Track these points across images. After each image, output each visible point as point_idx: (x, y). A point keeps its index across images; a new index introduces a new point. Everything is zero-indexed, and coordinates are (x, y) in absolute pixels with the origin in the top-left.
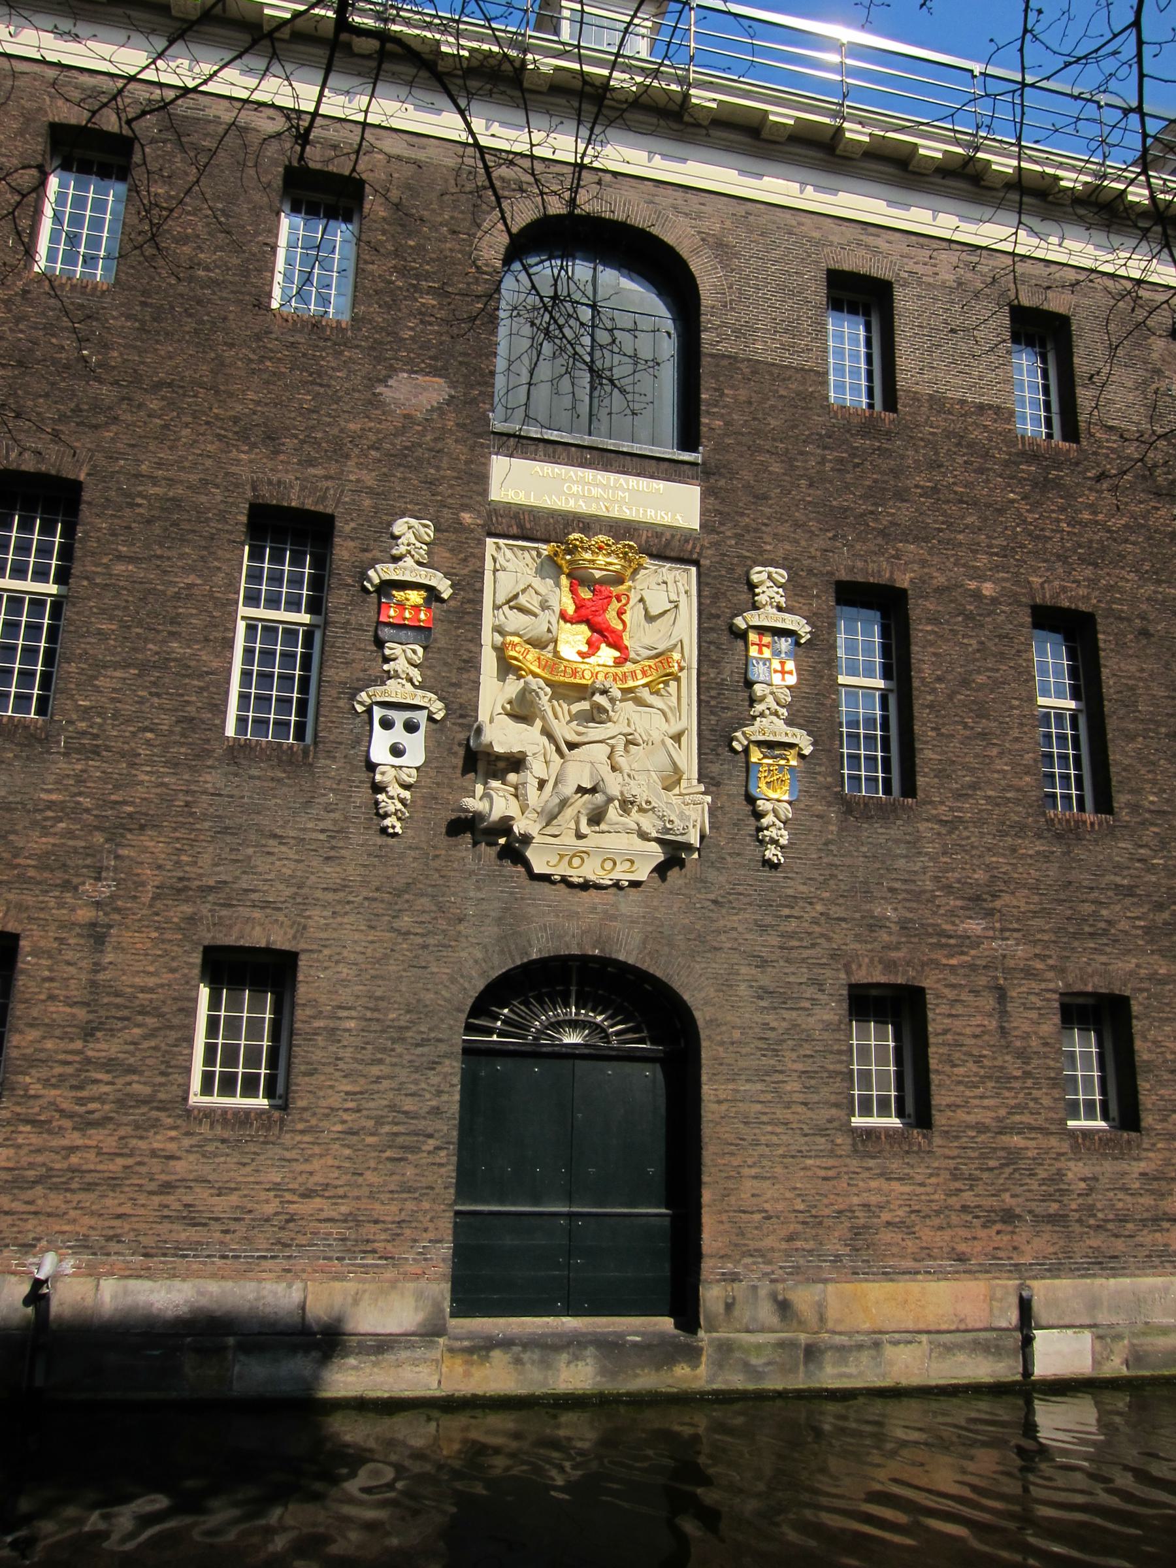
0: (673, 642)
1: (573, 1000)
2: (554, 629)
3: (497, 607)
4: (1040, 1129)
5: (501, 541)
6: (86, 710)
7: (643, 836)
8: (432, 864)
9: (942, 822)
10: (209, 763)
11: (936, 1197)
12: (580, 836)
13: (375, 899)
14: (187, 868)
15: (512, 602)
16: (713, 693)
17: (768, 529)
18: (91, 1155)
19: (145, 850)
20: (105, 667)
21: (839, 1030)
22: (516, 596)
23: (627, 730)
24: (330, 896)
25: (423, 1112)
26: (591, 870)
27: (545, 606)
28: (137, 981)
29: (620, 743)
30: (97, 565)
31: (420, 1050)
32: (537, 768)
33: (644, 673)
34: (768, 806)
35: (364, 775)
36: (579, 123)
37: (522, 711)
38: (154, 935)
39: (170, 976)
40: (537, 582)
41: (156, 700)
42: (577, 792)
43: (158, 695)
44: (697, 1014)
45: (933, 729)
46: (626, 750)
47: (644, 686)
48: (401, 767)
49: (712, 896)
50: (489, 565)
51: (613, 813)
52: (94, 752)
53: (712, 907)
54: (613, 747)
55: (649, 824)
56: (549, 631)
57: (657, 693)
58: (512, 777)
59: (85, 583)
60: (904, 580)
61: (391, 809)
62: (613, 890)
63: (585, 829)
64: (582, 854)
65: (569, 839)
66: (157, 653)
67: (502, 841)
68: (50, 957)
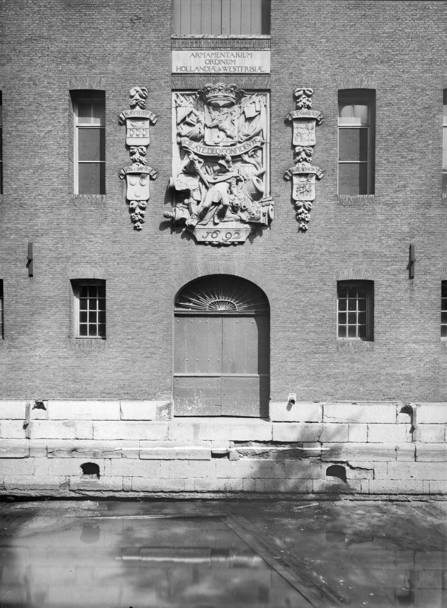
1: (262, 375)
2: (202, 133)
3: (178, 124)
4: (427, 341)
5: (178, 93)
6: (16, 189)
8: (156, 241)
9: (387, 204)
10: (64, 206)
11: (374, 369)
12: (215, 224)
13: (134, 257)
14: (61, 250)
16: (277, 153)
17: (304, 68)
18: (37, 358)
19: (45, 243)
20: (20, 170)
21: (332, 300)
22: (185, 118)
23: (237, 175)
24: (116, 257)
26: (220, 238)
28: (47, 294)
29: (234, 181)
30: (12, 127)
31: (154, 316)
32: (196, 195)
33: (245, 147)
34: (301, 204)
35: (125, 206)
36: (172, 201)
37: (190, 171)
38: (52, 276)
39: (59, 291)
40: (195, 111)
41: (41, 182)
43: (41, 180)
45: (385, 160)
46: (237, 184)
48: (140, 201)
49: (276, 246)
50: (174, 105)
51: (228, 213)
52: (21, 206)
53: (276, 250)
54: (230, 183)
55: (245, 216)
56: (200, 133)
57: (252, 156)
58: (186, 201)
59: (8, 136)
60: (372, 85)
61: (137, 219)
62: (232, 246)
63: (217, 221)
64: (216, 232)
66: (39, 162)
67: (184, 229)
68: (15, 287)
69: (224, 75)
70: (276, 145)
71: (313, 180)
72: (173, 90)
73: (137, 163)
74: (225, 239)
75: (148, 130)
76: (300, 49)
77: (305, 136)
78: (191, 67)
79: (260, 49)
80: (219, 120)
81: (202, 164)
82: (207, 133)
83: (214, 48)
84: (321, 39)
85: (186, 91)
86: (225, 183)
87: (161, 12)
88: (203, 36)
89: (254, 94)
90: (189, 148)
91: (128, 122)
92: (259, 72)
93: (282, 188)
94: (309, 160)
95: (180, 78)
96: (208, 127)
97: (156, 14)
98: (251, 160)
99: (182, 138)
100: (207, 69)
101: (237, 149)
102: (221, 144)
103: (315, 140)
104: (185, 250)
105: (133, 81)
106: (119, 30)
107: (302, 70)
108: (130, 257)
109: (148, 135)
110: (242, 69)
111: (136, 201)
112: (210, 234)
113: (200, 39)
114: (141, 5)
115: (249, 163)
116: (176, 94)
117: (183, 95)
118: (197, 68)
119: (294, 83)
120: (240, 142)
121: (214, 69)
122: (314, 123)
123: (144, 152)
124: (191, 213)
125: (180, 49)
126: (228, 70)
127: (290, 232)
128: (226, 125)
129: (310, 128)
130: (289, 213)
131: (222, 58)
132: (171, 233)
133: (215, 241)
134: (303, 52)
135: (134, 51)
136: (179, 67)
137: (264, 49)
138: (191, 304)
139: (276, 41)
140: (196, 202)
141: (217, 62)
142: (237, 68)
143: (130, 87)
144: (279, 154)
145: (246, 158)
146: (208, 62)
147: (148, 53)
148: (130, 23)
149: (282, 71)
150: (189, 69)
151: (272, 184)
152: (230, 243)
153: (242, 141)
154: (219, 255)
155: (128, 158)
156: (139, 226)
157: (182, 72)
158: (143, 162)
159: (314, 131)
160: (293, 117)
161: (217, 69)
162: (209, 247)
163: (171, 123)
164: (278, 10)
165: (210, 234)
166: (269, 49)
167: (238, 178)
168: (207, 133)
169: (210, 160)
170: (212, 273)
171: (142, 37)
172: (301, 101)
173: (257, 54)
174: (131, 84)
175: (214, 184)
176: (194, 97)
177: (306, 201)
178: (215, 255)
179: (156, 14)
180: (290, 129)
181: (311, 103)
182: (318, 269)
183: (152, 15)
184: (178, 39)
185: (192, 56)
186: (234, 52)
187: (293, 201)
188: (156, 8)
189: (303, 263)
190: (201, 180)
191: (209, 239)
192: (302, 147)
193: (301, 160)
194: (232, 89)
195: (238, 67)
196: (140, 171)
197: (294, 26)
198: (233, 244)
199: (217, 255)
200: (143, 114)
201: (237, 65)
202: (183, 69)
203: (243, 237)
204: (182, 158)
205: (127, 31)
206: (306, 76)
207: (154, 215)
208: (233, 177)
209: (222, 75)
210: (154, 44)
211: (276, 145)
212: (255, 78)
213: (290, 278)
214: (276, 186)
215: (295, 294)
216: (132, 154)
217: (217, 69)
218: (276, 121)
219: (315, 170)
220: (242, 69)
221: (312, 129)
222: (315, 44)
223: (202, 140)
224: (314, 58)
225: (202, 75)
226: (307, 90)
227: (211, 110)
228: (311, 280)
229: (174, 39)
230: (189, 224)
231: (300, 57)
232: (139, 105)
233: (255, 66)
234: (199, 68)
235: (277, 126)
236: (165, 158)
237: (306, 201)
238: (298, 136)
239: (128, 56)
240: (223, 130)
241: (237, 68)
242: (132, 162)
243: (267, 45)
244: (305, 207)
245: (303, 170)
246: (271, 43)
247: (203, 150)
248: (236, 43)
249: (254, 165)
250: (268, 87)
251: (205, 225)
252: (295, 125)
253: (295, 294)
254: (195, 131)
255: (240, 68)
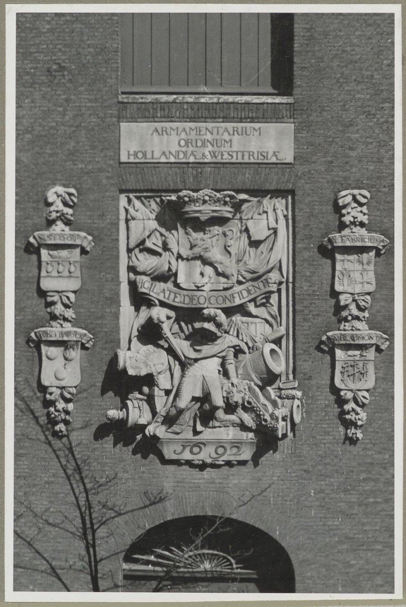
0: (270, 266)
5: (131, 196)
7: (243, 427)
12: (196, 433)
13: (52, 482)
15: (141, 246)
16: (306, 303)
17: (353, 154)
22: (143, 242)
25: (240, 410)
26: (206, 455)
27: (165, 247)
33: (249, 292)
37: (150, 334)
42: (192, 401)
44: (292, 557)
47: (250, 301)
49: (305, 467)
50: (122, 215)
53: (305, 475)
57: (263, 305)
61: (59, 419)
63: (199, 428)
64: (200, 445)
65: (189, 435)
69: (212, 165)
70: (305, 288)
71: (371, 354)
72: (122, 191)
73: (59, 321)
74: (214, 455)
75: (78, 265)
76: (347, 120)
77: (357, 276)
78: (153, 152)
79: (274, 120)
80: (204, 247)
81: (173, 320)
82: (182, 268)
83: (193, 119)
84: (383, 103)
85: (145, 193)
86: (215, 358)
87: (100, 57)
88: (175, 99)
89: (266, 196)
90: (151, 294)
91: (44, 252)
92: (274, 160)
93: (315, 363)
94: (364, 317)
95: (134, 170)
96: (183, 259)
97: (91, 61)
98: (262, 312)
99: (138, 277)
100: (181, 155)
101: (236, 295)
102: (206, 288)
103: (374, 282)
104: (143, 473)
105: (51, 176)
106: (27, 89)
107: (349, 157)
108: (46, 482)
109: (78, 273)
110: (243, 156)
111: (57, 387)
112: (188, 449)
113: (169, 103)
114: (65, 46)
115: (257, 317)
116: (126, 196)
117: (138, 198)
118: (164, 153)
119: (336, 179)
120: (240, 283)
121: (195, 156)
122: (372, 253)
123: (71, 303)
124: (154, 413)
125: (133, 119)
126: (220, 157)
127: (330, 443)
128: (216, 254)
129: (365, 261)
130: (329, 409)
131: (209, 137)
132: (115, 445)
133: (198, 458)
134: (351, 125)
135: (54, 124)
136: (132, 152)
137: (282, 120)
138: (152, 558)
139: (304, 106)
140: (163, 393)
141: (199, 144)
142: (234, 155)
143: (47, 188)
144: (311, 304)
145: (251, 308)
146: (183, 143)
147: (77, 127)
148: (47, 76)
149: (314, 158)
150: (149, 155)
151: (297, 357)
152: (223, 463)
153: (244, 281)
154: (203, 481)
155: (43, 312)
156: (61, 431)
157: (137, 161)
158: (70, 318)
159: (372, 267)
160: (335, 245)
161: (199, 155)
162: (186, 467)
163: (118, 248)
164: (307, 52)
165: (188, 449)
166: (292, 120)
167: (237, 348)
168: (182, 268)
169: (188, 315)
170: (191, 513)
171: (67, 100)
172: (348, 213)
173: (271, 128)
174: (49, 182)
175: (196, 360)
176: (158, 200)
177: (359, 390)
178: (197, 481)
179: (91, 61)
180: (329, 261)
181: (366, 217)
182: (379, 509)
183: (85, 62)
184: (130, 103)
185: (155, 134)
186: (230, 126)
187: (335, 391)
188: (91, 50)
189: (354, 498)
190: (171, 351)
191: (187, 455)
192: (352, 294)
193: (350, 318)
194: (228, 199)
195: (237, 152)
196: (65, 338)
197: (335, 81)
198: (229, 464)
199: (201, 481)
200: (69, 239)
201: (235, 148)
202: (140, 155)
203: (247, 454)
204: (137, 310)
205: (41, 90)
206: (356, 167)
207: (89, 411)
208: (229, 347)
209: (207, 165)
210: (89, 112)
211: (305, 288)
212: (267, 170)
213: (330, 523)
214: (305, 361)
215: (338, 552)
216: (50, 304)
217: (199, 155)
218: (304, 246)
219: (375, 338)
220: (243, 156)
221: (368, 263)
222: (373, 112)
223: (172, 279)
224: (370, 137)
225: (173, 165)
226: (360, 194)
227: (190, 230)
228: (367, 528)
229: (123, 103)
230: (152, 434)
231: (347, 135)
232: (62, 220)
233: (265, 150)
234: (167, 154)
235: (306, 254)
236: (107, 310)
237: (359, 390)
238: (343, 274)
239: (43, 133)
240: (211, 264)
241: (234, 155)
242: (48, 317)
243: (288, 113)
244: (355, 400)
245: (353, 340)
246: (293, 111)
247: (175, 297)
248: (232, 109)
249: (267, 321)
250: (290, 186)
251: (178, 434)
252: (338, 257)
253: (338, 552)
254: (161, 263)
255: (240, 155)
